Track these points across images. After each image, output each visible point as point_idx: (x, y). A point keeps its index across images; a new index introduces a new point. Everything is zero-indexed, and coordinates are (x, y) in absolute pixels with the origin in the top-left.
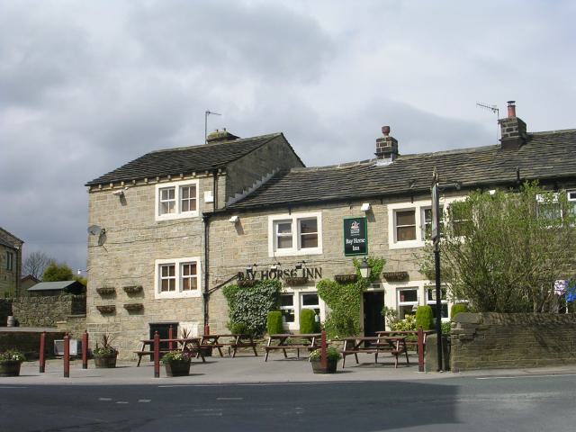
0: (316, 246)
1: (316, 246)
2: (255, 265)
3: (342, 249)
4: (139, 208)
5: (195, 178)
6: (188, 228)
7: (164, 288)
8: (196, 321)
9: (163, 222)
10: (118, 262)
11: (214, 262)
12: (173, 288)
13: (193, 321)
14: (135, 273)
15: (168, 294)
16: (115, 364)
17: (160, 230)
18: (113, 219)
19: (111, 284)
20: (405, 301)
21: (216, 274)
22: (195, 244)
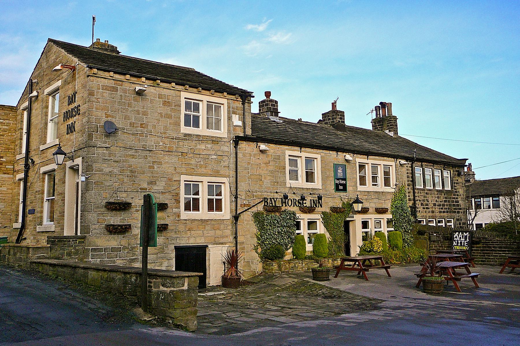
0: (368, 221)
1: (368, 221)
2: (277, 192)
3: (333, 187)
4: (161, 114)
5: (225, 97)
6: (216, 147)
7: (187, 208)
8: (225, 243)
9: (189, 135)
10: (131, 171)
11: (243, 186)
12: (196, 208)
13: (222, 244)
14: (155, 187)
15: (192, 214)
16: (345, 178)
17: (186, 142)
18: (126, 118)
19: (123, 197)
20: (367, 221)
21: (243, 197)
22: (222, 164)
